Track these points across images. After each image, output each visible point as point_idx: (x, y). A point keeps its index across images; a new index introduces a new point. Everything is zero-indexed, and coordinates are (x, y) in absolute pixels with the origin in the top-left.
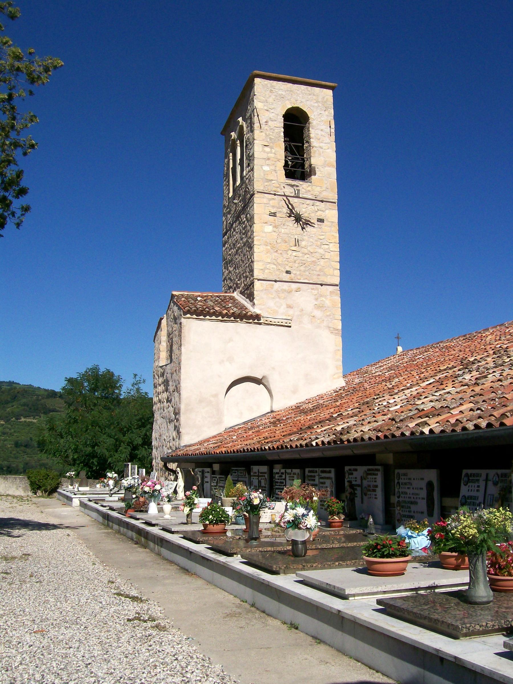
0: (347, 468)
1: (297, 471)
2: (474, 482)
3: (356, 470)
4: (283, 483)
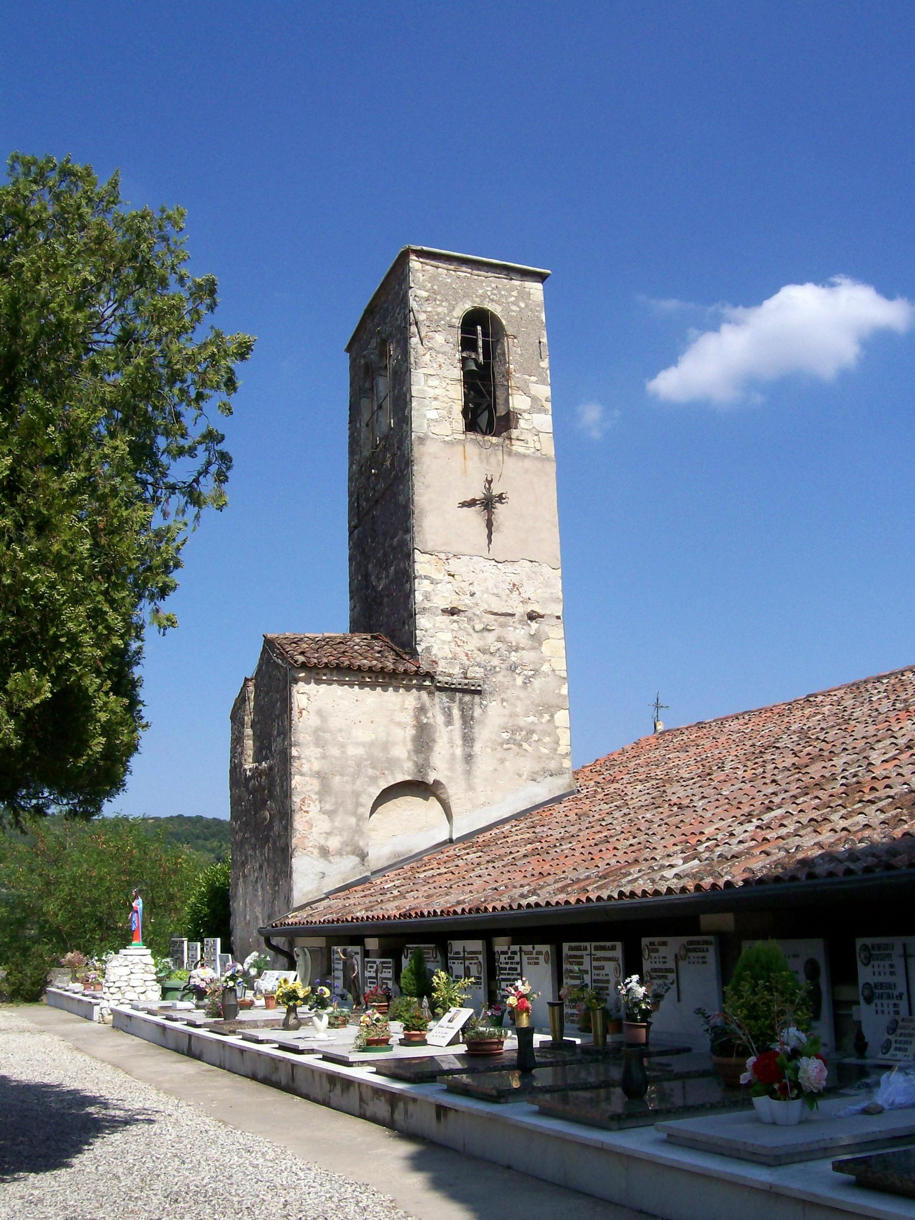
0: (645, 941)
1: (546, 948)
2: (882, 960)
3: (664, 944)
4: (516, 969)
